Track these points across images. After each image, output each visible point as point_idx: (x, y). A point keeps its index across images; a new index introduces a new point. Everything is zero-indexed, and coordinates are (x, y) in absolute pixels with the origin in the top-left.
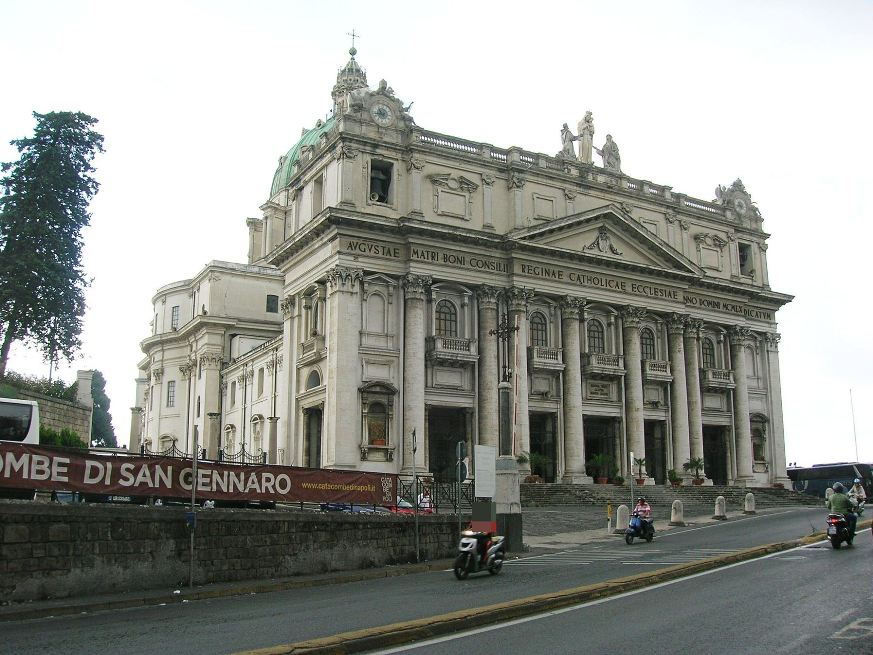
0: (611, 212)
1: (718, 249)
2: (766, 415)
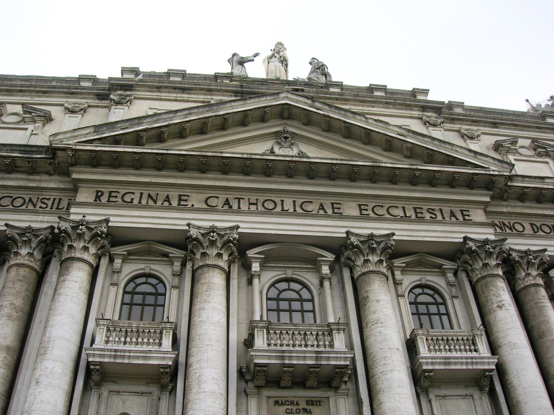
1: (547, 160)
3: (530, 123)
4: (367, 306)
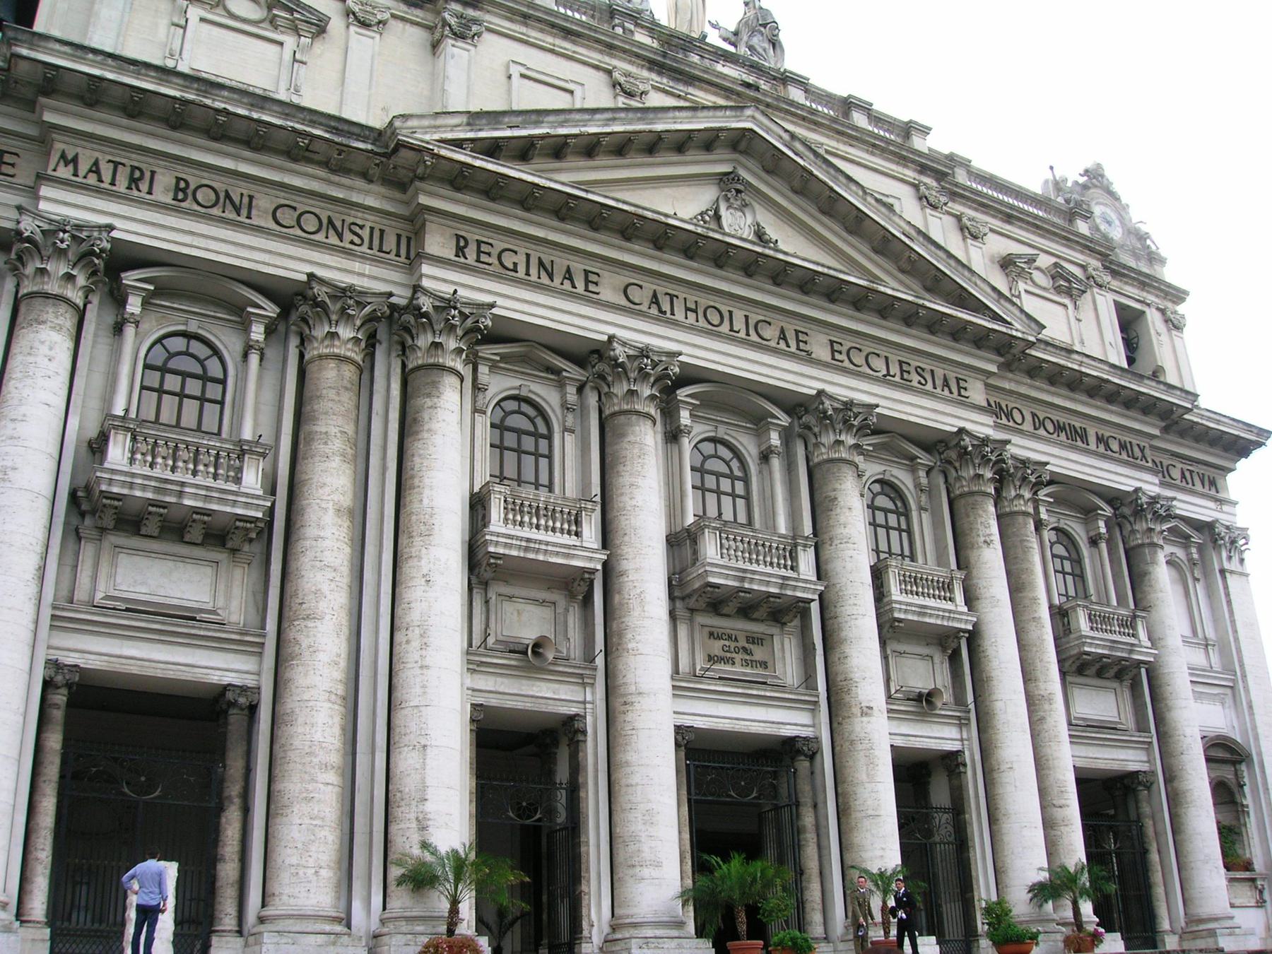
0: (751, 130)
1: (1067, 301)
2: (1239, 740)
3: (1058, 228)
4: (833, 513)
